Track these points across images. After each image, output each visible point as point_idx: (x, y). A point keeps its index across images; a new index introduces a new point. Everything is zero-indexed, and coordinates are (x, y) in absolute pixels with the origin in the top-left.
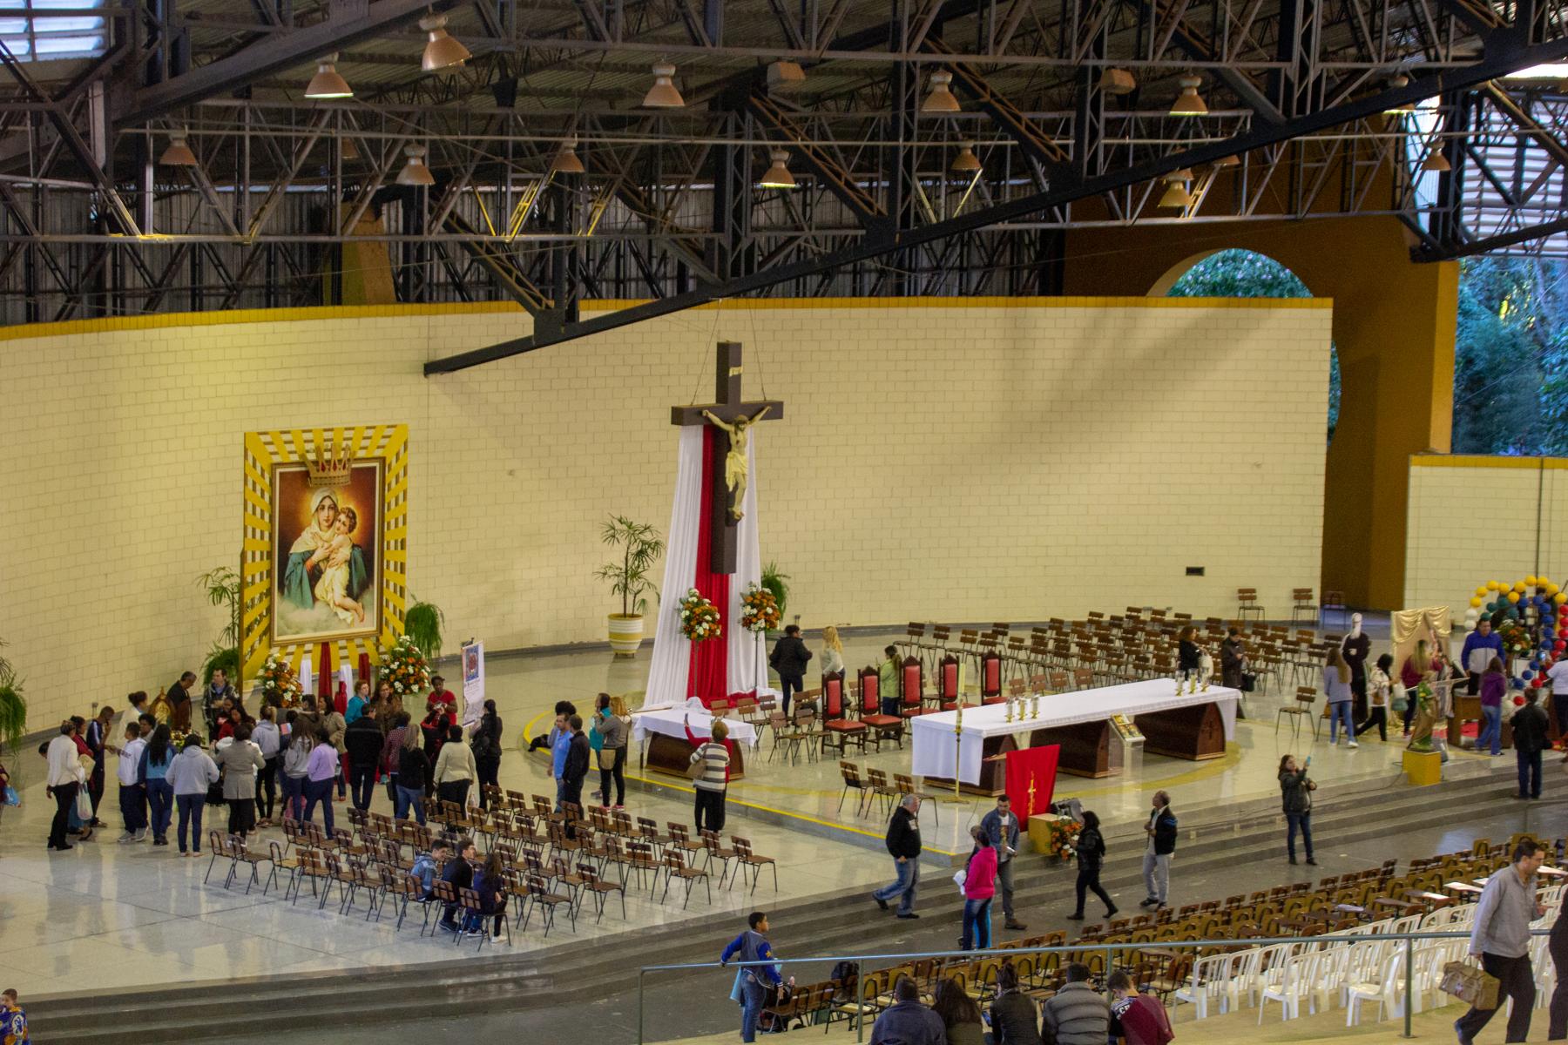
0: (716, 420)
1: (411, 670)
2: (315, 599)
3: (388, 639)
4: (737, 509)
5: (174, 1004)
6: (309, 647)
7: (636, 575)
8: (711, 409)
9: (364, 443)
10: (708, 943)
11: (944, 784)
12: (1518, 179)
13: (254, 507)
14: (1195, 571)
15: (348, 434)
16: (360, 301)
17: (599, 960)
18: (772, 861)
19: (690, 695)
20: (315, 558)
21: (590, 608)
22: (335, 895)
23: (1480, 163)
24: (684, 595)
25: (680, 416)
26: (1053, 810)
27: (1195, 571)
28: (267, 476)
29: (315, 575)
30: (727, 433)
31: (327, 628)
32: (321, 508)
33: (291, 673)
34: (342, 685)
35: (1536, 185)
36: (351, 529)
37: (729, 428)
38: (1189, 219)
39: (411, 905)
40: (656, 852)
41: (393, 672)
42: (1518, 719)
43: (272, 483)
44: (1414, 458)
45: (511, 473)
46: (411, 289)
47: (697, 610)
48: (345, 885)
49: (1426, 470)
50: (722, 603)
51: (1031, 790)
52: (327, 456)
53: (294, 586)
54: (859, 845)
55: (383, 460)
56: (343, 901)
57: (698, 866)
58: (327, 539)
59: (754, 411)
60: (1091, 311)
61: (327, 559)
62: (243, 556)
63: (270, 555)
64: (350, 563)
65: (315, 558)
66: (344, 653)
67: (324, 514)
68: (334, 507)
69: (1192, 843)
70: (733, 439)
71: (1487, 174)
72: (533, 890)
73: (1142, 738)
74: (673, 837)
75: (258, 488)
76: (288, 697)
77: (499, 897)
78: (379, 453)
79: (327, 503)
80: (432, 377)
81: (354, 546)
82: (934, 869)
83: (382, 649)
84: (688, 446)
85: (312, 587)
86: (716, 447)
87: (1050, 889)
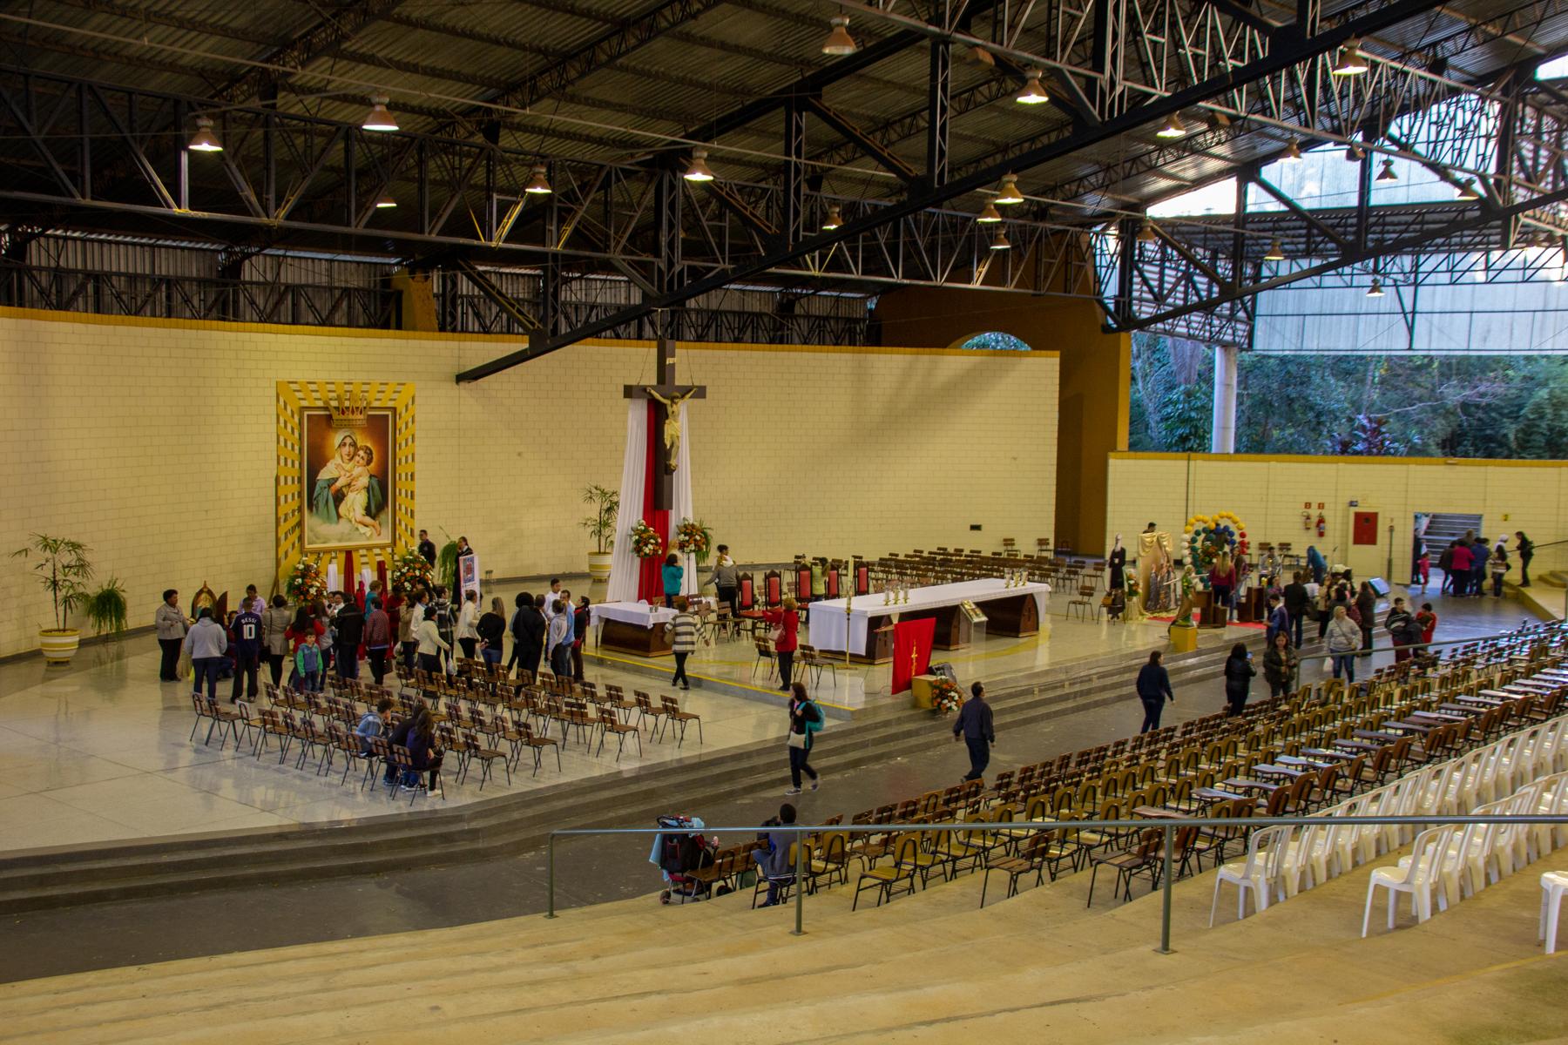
0: (657, 396)
2: (339, 517)
3: (401, 548)
4: (673, 462)
5: (108, 864)
7: (607, 525)
8: (653, 387)
9: (379, 396)
10: (637, 794)
11: (837, 655)
12: (1161, 287)
14: (976, 528)
15: (365, 388)
16: (414, 329)
17: (530, 812)
18: (697, 717)
19: (640, 598)
20: (338, 484)
21: (575, 551)
23: (1141, 274)
24: (635, 525)
25: (629, 392)
26: (931, 671)
27: (976, 528)
29: (339, 497)
32: (343, 444)
33: (317, 574)
34: (361, 584)
35: (1171, 291)
36: (369, 462)
37: (667, 402)
38: (976, 285)
40: (592, 711)
41: (403, 574)
42: (1304, 592)
43: (301, 423)
44: (1111, 454)
46: (447, 323)
49: (1119, 462)
50: (663, 529)
51: (914, 656)
52: (347, 404)
53: (321, 505)
54: (772, 703)
55: (394, 409)
57: (632, 723)
58: (346, 469)
59: (685, 391)
60: (908, 357)
61: (349, 485)
62: (277, 479)
65: (338, 484)
66: (365, 560)
67: (346, 449)
68: (354, 444)
69: (1037, 698)
70: (670, 410)
71: (1145, 281)
72: (468, 746)
73: (984, 619)
74: (610, 697)
76: (313, 591)
77: (432, 753)
78: (391, 404)
79: (348, 441)
80: (462, 384)
82: (837, 722)
84: (636, 417)
85: (337, 507)
86: (657, 416)
87: (933, 737)
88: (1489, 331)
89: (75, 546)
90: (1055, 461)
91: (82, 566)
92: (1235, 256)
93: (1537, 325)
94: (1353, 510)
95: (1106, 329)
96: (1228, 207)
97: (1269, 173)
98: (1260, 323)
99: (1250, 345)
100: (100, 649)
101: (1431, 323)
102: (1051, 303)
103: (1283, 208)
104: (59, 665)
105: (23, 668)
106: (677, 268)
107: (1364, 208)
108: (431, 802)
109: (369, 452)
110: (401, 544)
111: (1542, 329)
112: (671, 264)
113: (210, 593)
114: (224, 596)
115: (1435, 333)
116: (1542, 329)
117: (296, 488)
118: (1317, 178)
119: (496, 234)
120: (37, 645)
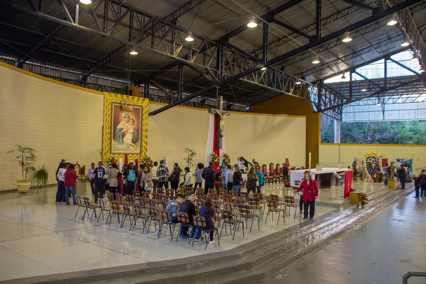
1: (149, 163)
2: (123, 142)
6: (122, 155)
7: (191, 159)
13: (106, 120)
20: (123, 131)
22: (127, 222)
28: (110, 105)
29: (123, 135)
30: (220, 116)
31: (126, 151)
32: (125, 117)
37: (221, 115)
39: (165, 225)
45: (165, 138)
47: (215, 156)
48: (132, 218)
49: (321, 146)
53: (118, 137)
55: (142, 107)
56: (131, 225)
61: (127, 131)
63: (111, 128)
64: (133, 133)
65: (123, 131)
66: (131, 158)
67: (126, 119)
68: (129, 117)
70: (221, 117)
75: (108, 114)
79: (127, 116)
80: (150, 116)
81: (134, 129)
83: (141, 158)
88: (404, 115)
89: (31, 150)
90: (305, 146)
91: (33, 157)
92: (348, 93)
93: (416, 113)
94: (381, 158)
95: (314, 112)
96: (347, 79)
97: (358, 70)
98: (343, 115)
99: (341, 119)
100: (39, 190)
101: (389, 113)
102: (297, 106)
103: (363, 79)
104: (23, 193)
105: (11, 195)
106: (223, 75)
107: (385, 79)
108: (211, 248)
109: (134, 121)
110: (143, 153)
111: (418, 114)
112: (221, 73)
113: (79, 165)
114: (84, 167)
115: (390, 116)
116: (418, 114)
117: (109, 130)
118: (373, 71)
119: (175, 53)
120: (16, 187)
